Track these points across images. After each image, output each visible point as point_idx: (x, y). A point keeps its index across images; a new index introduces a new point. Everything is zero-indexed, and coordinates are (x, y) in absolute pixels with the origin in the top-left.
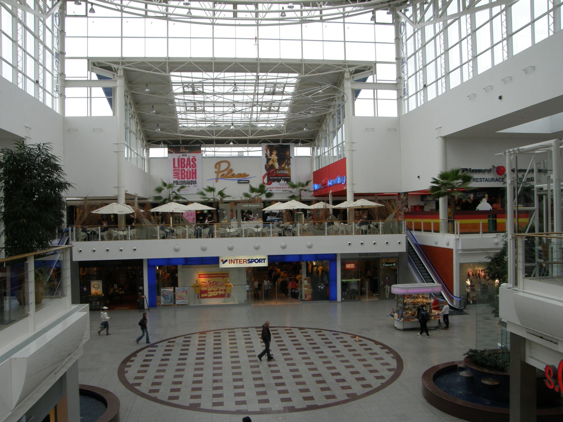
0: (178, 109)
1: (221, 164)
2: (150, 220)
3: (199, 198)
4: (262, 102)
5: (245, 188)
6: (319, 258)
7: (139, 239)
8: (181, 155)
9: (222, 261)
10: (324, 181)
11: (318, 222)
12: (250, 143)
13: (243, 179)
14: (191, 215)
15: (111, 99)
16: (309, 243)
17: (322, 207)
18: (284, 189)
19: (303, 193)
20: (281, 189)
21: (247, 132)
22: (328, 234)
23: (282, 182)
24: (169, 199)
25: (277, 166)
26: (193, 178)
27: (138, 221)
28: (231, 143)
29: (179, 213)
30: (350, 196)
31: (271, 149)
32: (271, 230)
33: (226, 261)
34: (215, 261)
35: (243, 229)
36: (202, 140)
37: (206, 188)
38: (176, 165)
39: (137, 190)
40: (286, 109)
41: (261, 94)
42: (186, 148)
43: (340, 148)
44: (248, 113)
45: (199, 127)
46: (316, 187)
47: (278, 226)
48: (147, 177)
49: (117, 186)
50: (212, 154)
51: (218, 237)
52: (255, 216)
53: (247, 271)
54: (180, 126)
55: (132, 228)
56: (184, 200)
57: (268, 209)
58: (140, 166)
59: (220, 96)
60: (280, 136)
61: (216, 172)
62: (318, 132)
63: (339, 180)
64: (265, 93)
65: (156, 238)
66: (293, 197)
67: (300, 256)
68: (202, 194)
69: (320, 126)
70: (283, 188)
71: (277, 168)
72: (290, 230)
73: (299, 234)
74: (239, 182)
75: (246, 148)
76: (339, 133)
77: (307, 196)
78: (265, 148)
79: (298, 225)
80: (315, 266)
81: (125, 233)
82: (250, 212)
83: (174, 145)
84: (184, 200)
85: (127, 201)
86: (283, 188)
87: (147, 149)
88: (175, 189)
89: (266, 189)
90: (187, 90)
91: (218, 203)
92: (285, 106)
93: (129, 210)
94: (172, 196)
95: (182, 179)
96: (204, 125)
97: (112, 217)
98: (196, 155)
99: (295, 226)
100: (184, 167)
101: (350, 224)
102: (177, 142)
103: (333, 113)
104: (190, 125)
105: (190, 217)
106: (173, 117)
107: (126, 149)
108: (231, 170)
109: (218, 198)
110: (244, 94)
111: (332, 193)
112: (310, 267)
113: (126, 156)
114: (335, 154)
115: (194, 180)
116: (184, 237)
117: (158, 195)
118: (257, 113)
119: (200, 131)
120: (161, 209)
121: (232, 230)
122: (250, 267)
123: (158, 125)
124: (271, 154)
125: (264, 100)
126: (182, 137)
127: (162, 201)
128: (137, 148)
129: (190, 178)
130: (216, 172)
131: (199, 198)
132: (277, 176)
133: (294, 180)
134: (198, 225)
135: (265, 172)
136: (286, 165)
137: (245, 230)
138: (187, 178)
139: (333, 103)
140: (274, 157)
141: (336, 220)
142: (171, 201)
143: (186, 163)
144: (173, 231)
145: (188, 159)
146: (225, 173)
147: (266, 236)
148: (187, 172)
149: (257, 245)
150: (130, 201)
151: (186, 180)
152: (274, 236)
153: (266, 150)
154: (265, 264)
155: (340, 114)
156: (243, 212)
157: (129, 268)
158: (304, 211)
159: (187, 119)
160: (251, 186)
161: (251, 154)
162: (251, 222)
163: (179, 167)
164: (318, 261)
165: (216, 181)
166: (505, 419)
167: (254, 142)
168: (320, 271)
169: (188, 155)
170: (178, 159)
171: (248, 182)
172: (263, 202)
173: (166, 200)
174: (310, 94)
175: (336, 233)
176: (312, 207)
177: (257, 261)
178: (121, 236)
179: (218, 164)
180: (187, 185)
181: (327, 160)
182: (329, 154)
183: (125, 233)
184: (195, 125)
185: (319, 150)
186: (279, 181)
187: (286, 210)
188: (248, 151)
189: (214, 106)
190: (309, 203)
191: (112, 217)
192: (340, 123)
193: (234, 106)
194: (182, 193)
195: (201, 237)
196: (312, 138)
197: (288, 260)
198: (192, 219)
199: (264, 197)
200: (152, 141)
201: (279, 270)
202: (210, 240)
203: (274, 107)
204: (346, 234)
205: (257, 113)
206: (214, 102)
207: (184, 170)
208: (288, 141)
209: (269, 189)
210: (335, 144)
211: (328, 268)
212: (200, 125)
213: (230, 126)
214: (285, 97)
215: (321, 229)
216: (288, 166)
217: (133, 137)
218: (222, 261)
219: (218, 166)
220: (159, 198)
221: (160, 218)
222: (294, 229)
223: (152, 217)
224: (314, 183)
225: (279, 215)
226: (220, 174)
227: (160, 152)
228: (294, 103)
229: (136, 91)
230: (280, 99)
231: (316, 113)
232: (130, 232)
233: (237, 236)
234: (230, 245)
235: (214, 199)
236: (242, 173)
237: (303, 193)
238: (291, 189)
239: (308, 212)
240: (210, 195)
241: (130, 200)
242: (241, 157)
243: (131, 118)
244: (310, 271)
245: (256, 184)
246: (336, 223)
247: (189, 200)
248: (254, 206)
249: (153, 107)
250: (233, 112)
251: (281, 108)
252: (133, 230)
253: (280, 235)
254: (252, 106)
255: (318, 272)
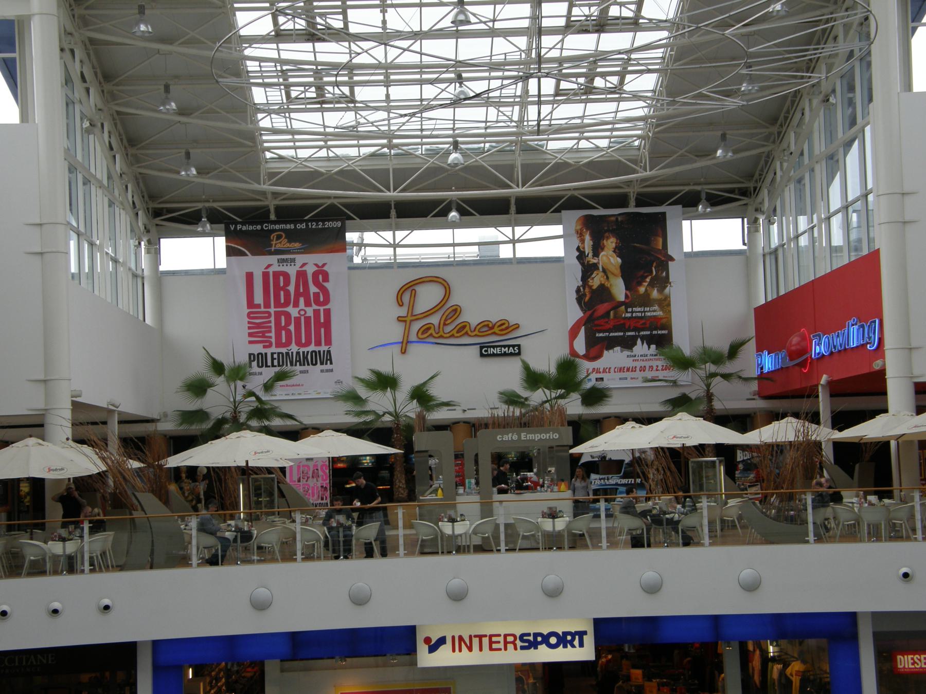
0: (258, 95)
1: (418, 288)
2: (165, 498)
3: (342, 414)
4: (561, 61)
5: (509, 375)
6: (784, 626)
7: (121, 568)
8: (273, 259)
9: (427, 640)
10: (795, 340)
11: (783, 496)
12: (519, 212)
13: (497, 341)
14: (315, 475)
15: (14, 60)
16: (747, 574)
17: (791, 438)
18: (649, 375)
19: (718, 385)
20: (638, 374)
21: (508, 170)
22: (819, 539)
23: (640, 348)
24: (235, 419)
25: (619, 290)
26: (318, 343)
27: (119, 503)
28: (453, 214)
29: (269, 470)
30: (898, 393)
31: (596, 229)
32: (603, 524)
33: (442, 641)
34: (399, 641)
35: (501, 521)
36: (346, 206)
37: (367, 375)
38: (259, 298)
39: (114, 387)
40: (647, 83)
41: (553, 31)
42: (292, 236)
43: (854, 217)
44: (512, 105)
45: (338, 158)
46: (769, 363)
47: (628, 509)
48: (156, 343)
49: (42, 377)
50: (384, 254)
51: (410, 553)
52: (542, 473)
53: (519, 680)
54: (268, 155)
55: (97, 527)
56: (289, 422)
57: (590, 448)
58: (125, 302)
59: (405, 44)
60: (629, 183)
61: (400, 319)
62: (769, 159)
63: (853, 336)
64: (571, 27)
65: (183, 561)
66: (680, 403)
67: (716, 620)
68: (353, 397)
69: (780, 136)
70: (643, 369)
71: (622, 298)
72: (674, 524)
73: (706, 540)
74: (485, 352)
75: (508, 230)
76: (852, 159)
77: (734, 397)
78: (574, 225)
79: (704, 504)
80: (773, 659)
81: (71, 547)
82: (524, 462)
83: (250, 226)
84: (289, 422)
85: (80, 429)
86: (643, 369)
87: (149, 242)
88: (256, 382)
89: (582, 375)
90: (289, 26)
91: (409, 429)
92: (641, 72)
93: (84, 463)
94: (245, 410)
95: (279, 344)
96: (353, 152)
97: (25, 488)
98: (331, 261)
99: (694, 509)
100: (287, 304)
101: (903, 501)
102: (258, 215)
103: (825, 87)
104: (303, 154)
105: (311, 482)
106: (243, 126)
107: (73, 244)
108: (456, 311)
109: (411, 410)
110: (492, 33)
111: (830, 383)
112: (756, 662)
113: (73, 269)
114: (838, 239)
115: (323, 348)
116: (288, 556)
117: (192, 404)
118: (539, 103)
119: (342, 172)
120: (203, 456)
121: (460, 528)
122: (532, 666)
123: (188, 155)
124: (597, 249)
125: (566, 53)
126: (275, 195)
127: (207, 426)
128: (113, 239)
129: (308, 343)
130: (400, 319)
131: (342, 414)
132: (621, 327)
133: (684, 340)
134: (339, 512)
135: (575, 313)
136: (652, 285)
137: (507, 526)
138: (299, 343)
139: (828, 49)
140: (610, 258)
141: (849, 487)
142: (238, 426)
143: (292, 288)
144: (246, 537)
145: (301, 275)
146: (435, 320)
147: (585, 547)
148: (297, 320)
149: (551, 580)
150: (92, 432)
151: (294, 348)
152: (613, 545)
153: (580, 235)
154: (584, 653)
155: (856, 87)
156: (498, 458)
157: (85, 678)
158: (725, 451)
159: (293, 132)
160: (526, 367)
161: (525, 251)
162: (528, 495)
163: (267, 305)
164: (783, 642)
165: (404, 352)
166: (899, 633)
167: (534, 208)
168: (796, 681)
169: (300, 259)
170: (265, 275)
171: (516, 351)
172: (570, 423)
173: (221, 422)
174: (738, 19)
175: (851, 534)
176: (753, 438)
177: (553, 640)
178: (55, 558)
179: (407, 292)
180: (298, 368)
181: (807, 260)
182: (813, 240)
183: (71, 547)
184: (323, 153)
185: (775, 228)
186: (628, 344)
187: (658, 451)
188: (513, 241)
189: (387, 83)
190: (741, 421)
191: (25, 488)
192: (853, 122)
193: (460, 79)
194: (280, 393)
195: (347, 553)
196: (751, 185)
197: (669, 635)
198: (316, 488)
199: (574, 406)
200: (169, 214)
201: (637, 673)
202: (377, 563)
203: (603, 75)
204: (891, 539)
205: (539, 103)
206: (387, 67)
207: (288, 315)
208: (660, 199)
209: (593, 376)
210: (836, 202)
211: (826, 667)
212: (340, 152)
213: (448, 153)
214: (643, 38)
215: (792, 520)
216: (661, 291)
217: (99, 200)
218: (427, 640)
219: (406, 298)
220: (200, 415)
221: (202, 487)
222: (689, 521)
223: (173, 487)
224: (760, 349)
225: (633, 468)
226: (416, 326)
227: (196, 253)
228: (677, 58)
229: (100, 30)
230: (627, 45)
231: (762, 89)
232: (90, 544)
233: (481, 549)
234: (456, 583)
235: (396, 415)
236: (494, 319)
237: (718, 385)
238: (673, 374)
239: (740, 456)
240: (380, 403)
241: (89, 426)
242: (488, 263)
243: (88, 131)
244: (757, 678)
245: (545, 355)
246: (850, 497)
247: (308, 421)
248: (537, 437)
249: (167, 88)
250: (456, 103)
251: (629, 78)
252: (99, 536)
253: (637, 542)
254: (525, 78)
255: (786, 683)
